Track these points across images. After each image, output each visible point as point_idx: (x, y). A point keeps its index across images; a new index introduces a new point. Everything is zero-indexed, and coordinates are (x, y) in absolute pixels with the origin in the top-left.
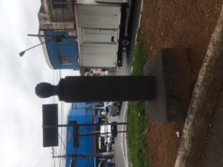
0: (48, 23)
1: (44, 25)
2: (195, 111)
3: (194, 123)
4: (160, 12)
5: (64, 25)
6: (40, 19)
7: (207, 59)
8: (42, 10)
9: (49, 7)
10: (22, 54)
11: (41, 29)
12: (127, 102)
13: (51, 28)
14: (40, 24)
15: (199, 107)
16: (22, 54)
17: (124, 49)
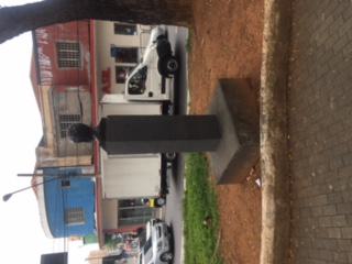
0: (50, 158)
1: (44, 163)
2: (267, 118)
3: (269, 136)
4: (212, 73)
5: (78, 161)
6: (38, 153)
7: (265, 57)
8: (43, 143)
9: (56, 136)
10: (7, 198)
11: (38, 168)
12: (188, 113)
13: (55, 165)
14: (38, 161)
15: (270, 113)
16: (7, 198)
17: (169, 164)
